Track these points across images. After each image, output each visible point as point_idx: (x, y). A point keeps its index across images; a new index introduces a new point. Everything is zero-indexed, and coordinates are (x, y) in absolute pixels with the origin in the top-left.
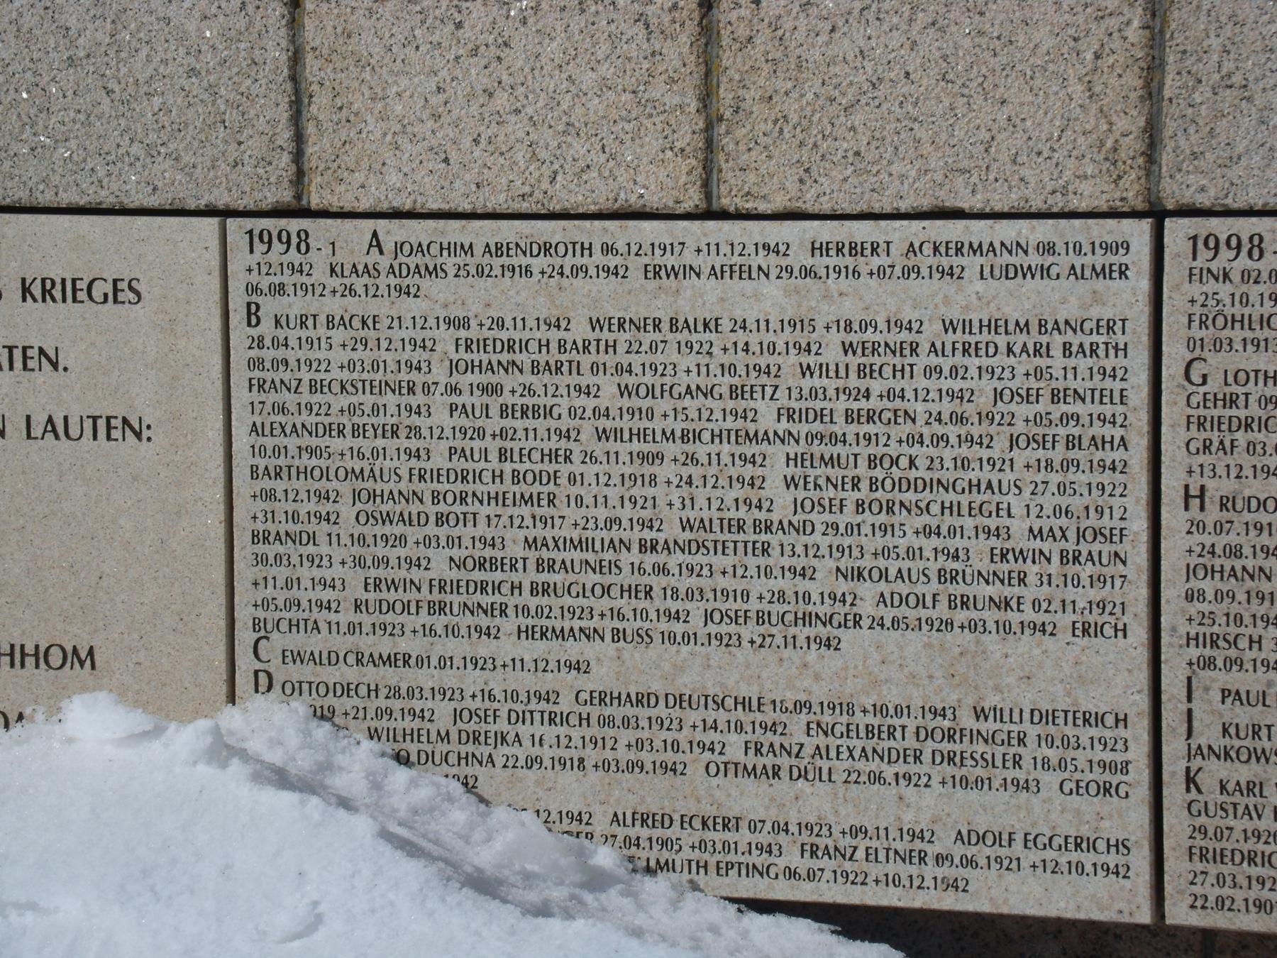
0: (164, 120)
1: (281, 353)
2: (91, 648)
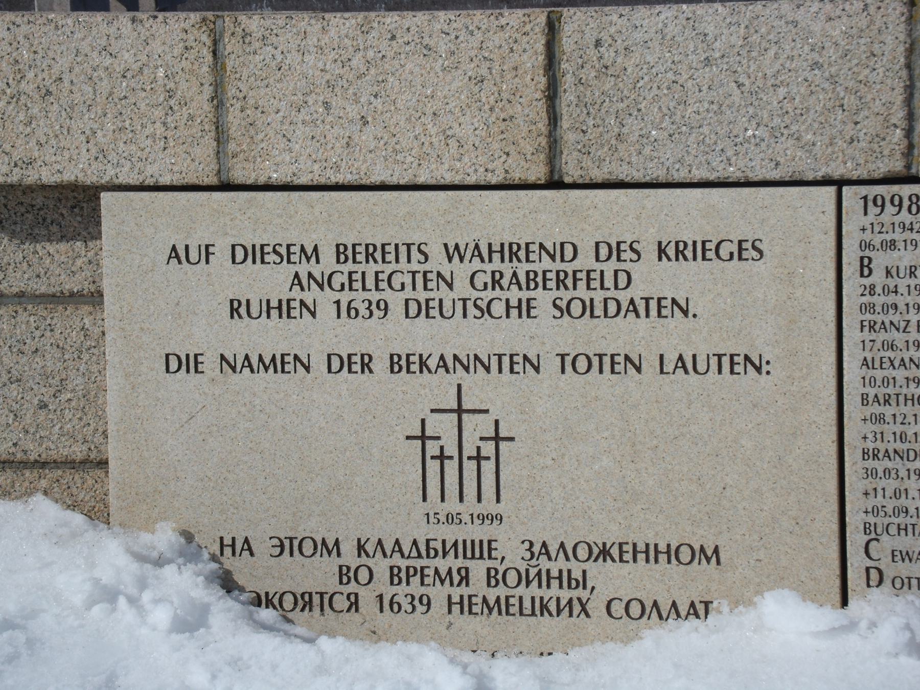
0: (788, 106)
1: (891, 299)
2: (717, 547)
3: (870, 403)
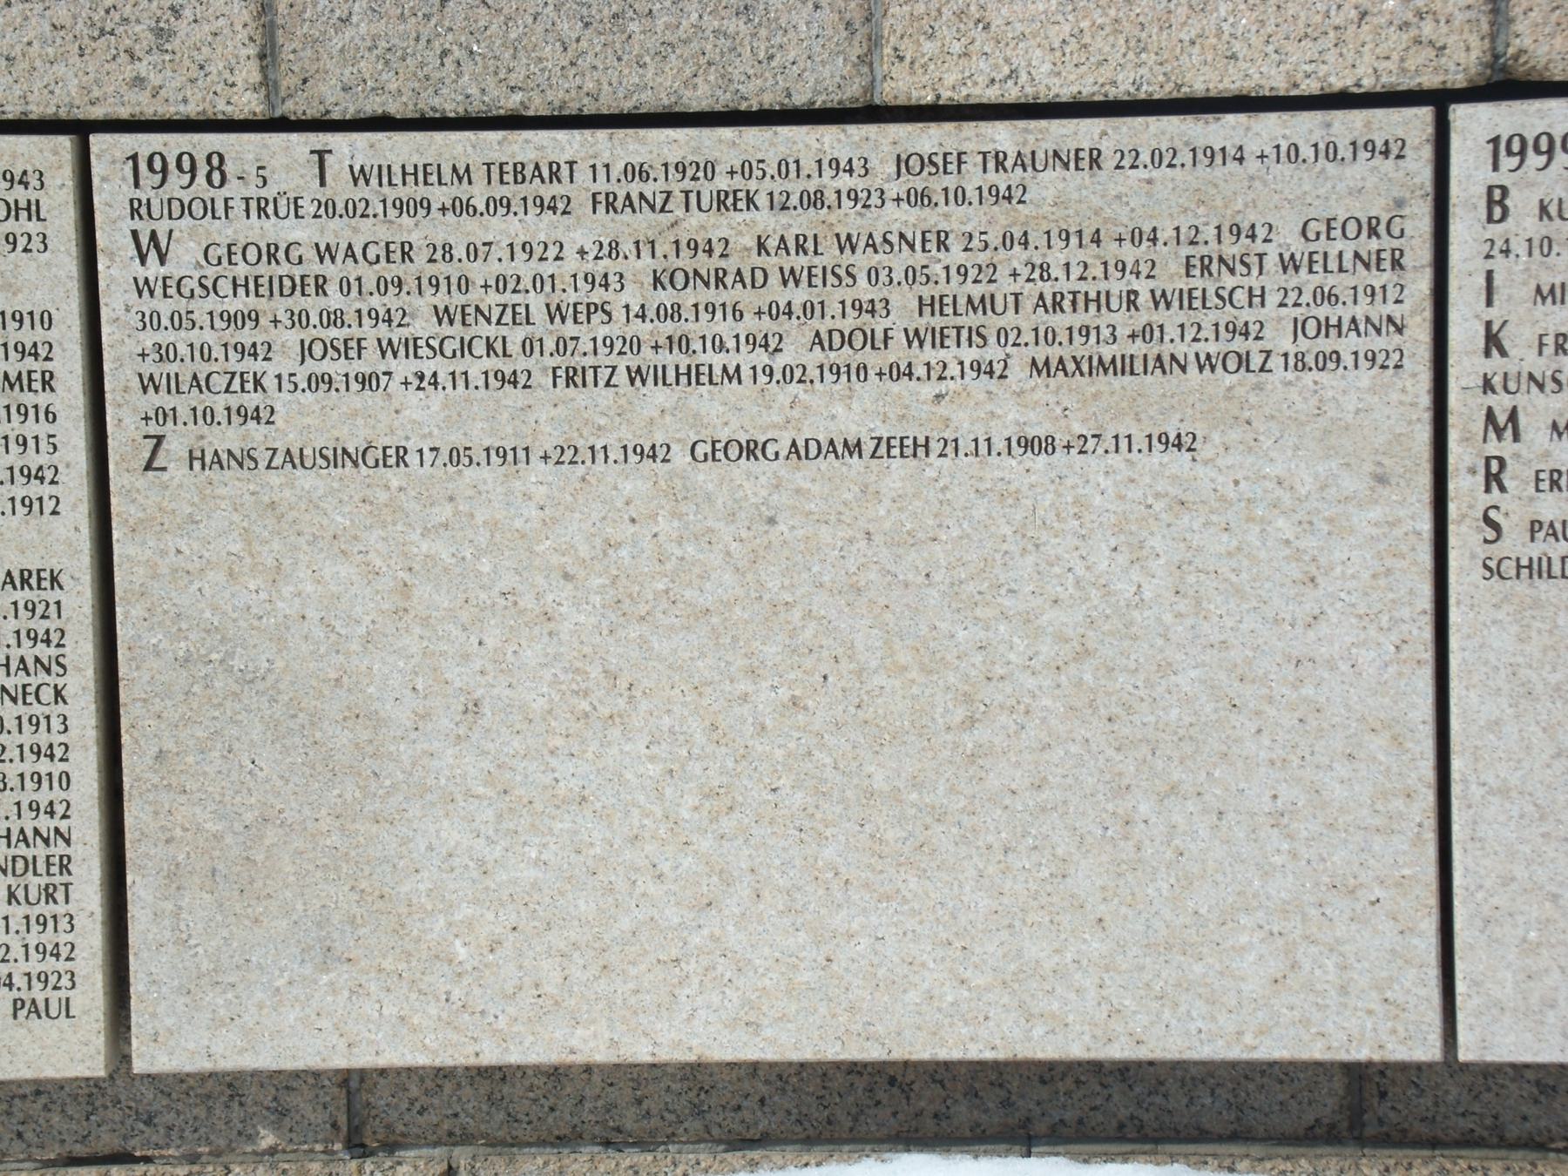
3: (528, 178)
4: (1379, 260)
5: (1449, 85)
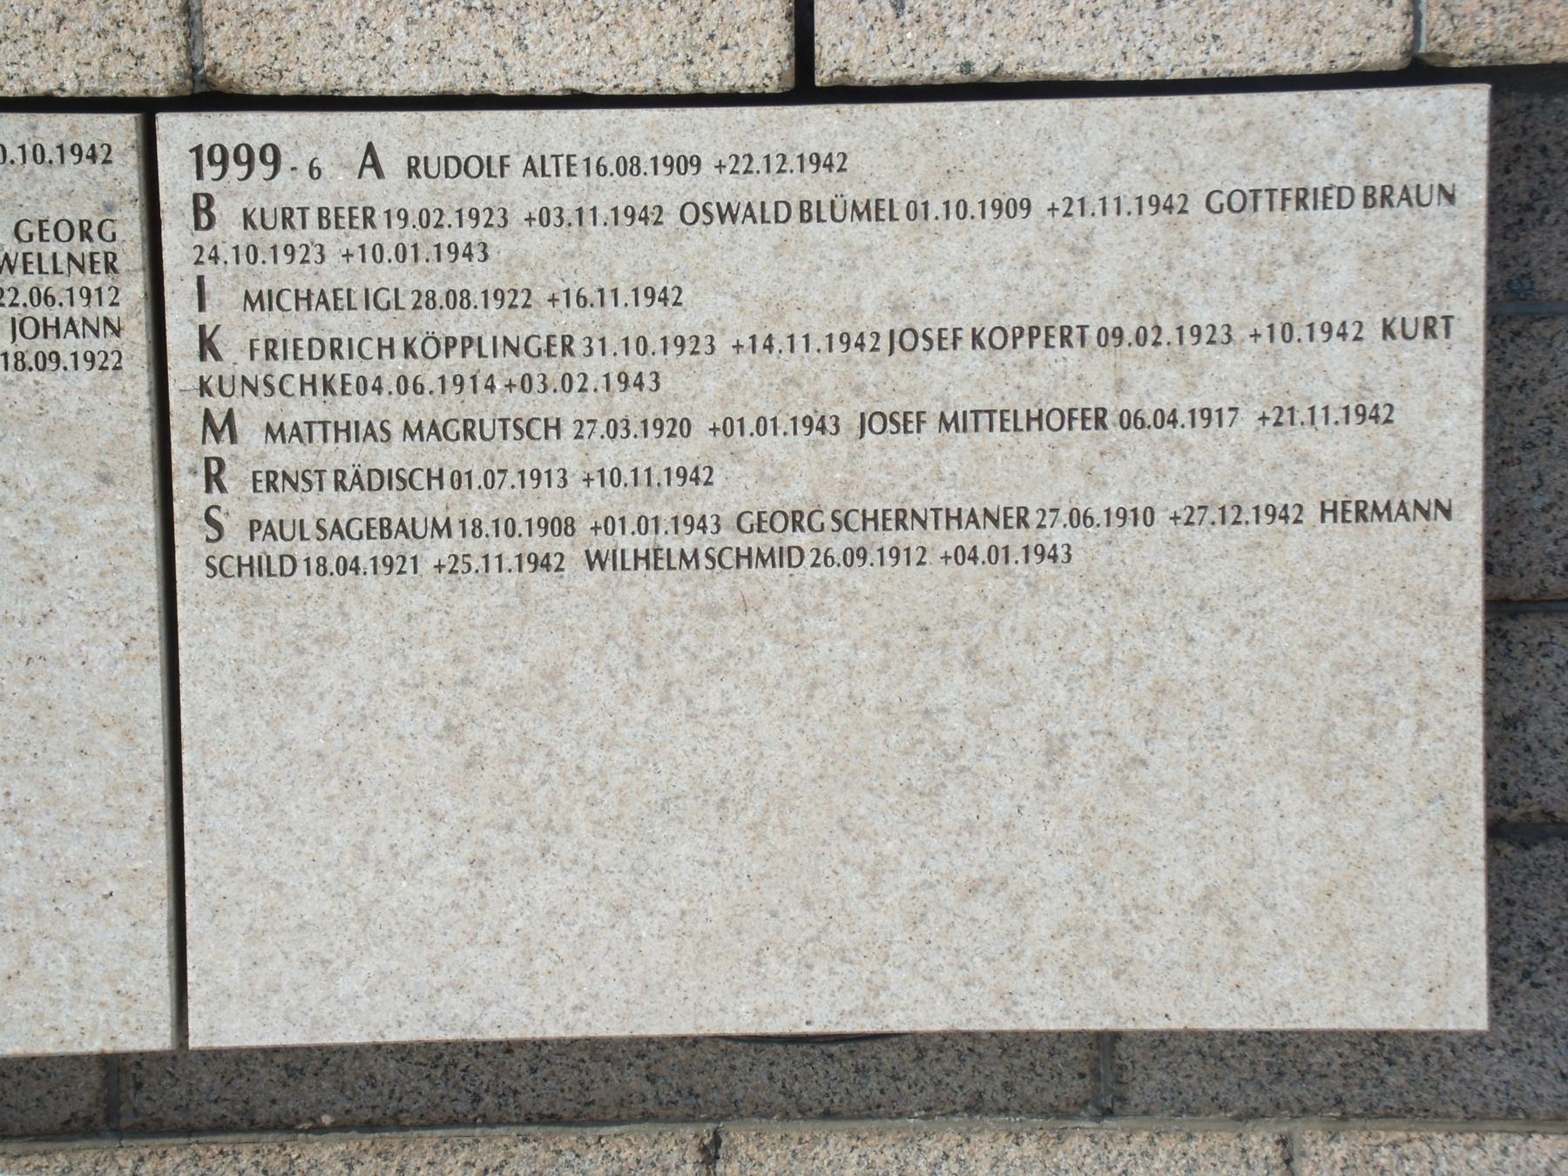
4: (93, 262)
5: (151, 94)
